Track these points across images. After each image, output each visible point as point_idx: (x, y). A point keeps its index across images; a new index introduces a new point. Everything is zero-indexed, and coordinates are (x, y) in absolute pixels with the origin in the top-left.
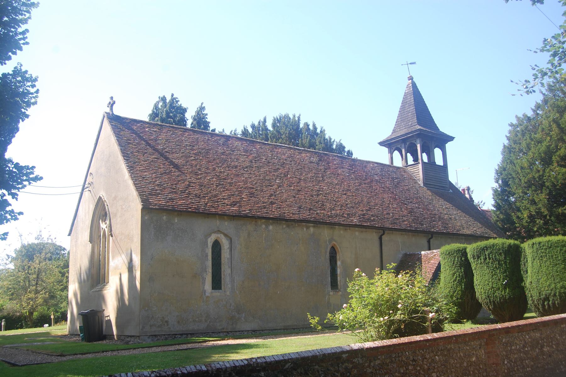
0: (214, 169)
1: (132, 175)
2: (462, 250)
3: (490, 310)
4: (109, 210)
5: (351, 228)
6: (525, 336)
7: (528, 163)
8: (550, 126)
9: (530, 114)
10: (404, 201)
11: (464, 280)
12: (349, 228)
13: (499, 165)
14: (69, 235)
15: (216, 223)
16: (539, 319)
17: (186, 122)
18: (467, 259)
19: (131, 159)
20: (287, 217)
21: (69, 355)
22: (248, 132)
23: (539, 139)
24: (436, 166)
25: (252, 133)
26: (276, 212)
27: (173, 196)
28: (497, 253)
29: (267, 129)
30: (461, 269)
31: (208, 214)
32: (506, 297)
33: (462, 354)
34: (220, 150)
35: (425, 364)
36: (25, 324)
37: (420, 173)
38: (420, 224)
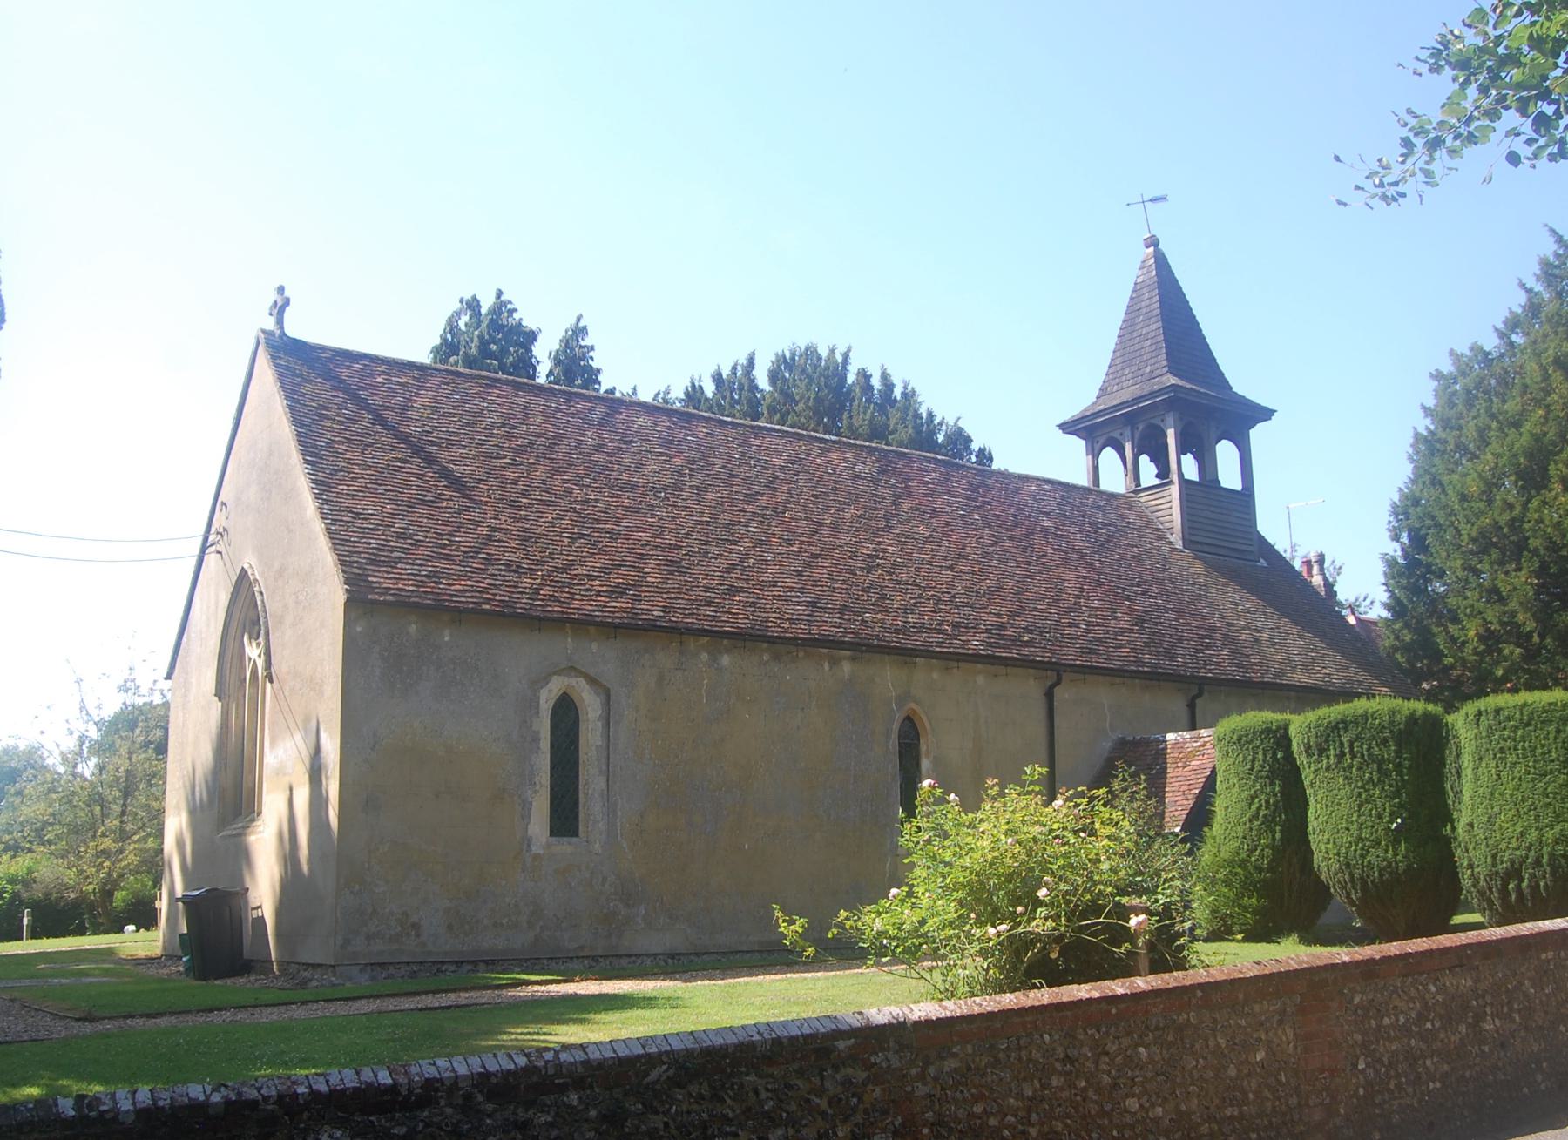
0: (569, 492)
1: (325, 507)
2: (1277, 731)
3: (1352, 903)
6: (1425, 986)
7: (1481, 484)
8: (1546, 377)
9: (1491, 343)
10: (1123, 590)
11: (1280, 816)
12: (956, 664)
13: (1401, 489)
15: (566, 645)
17: (535, 369)
18: (1290, 758)
19: (325, 462)
22: (703, 392)
23: (1513, 416)
24: (1223, 493)
26: (741, 616)
27: (440, 567)
29: (754, 388)
30: (1272, 784)
31: (540, 619)
32: (1397, 868)
35: (1104, 1072)
36: (91, 923)
37: (1173, 509)
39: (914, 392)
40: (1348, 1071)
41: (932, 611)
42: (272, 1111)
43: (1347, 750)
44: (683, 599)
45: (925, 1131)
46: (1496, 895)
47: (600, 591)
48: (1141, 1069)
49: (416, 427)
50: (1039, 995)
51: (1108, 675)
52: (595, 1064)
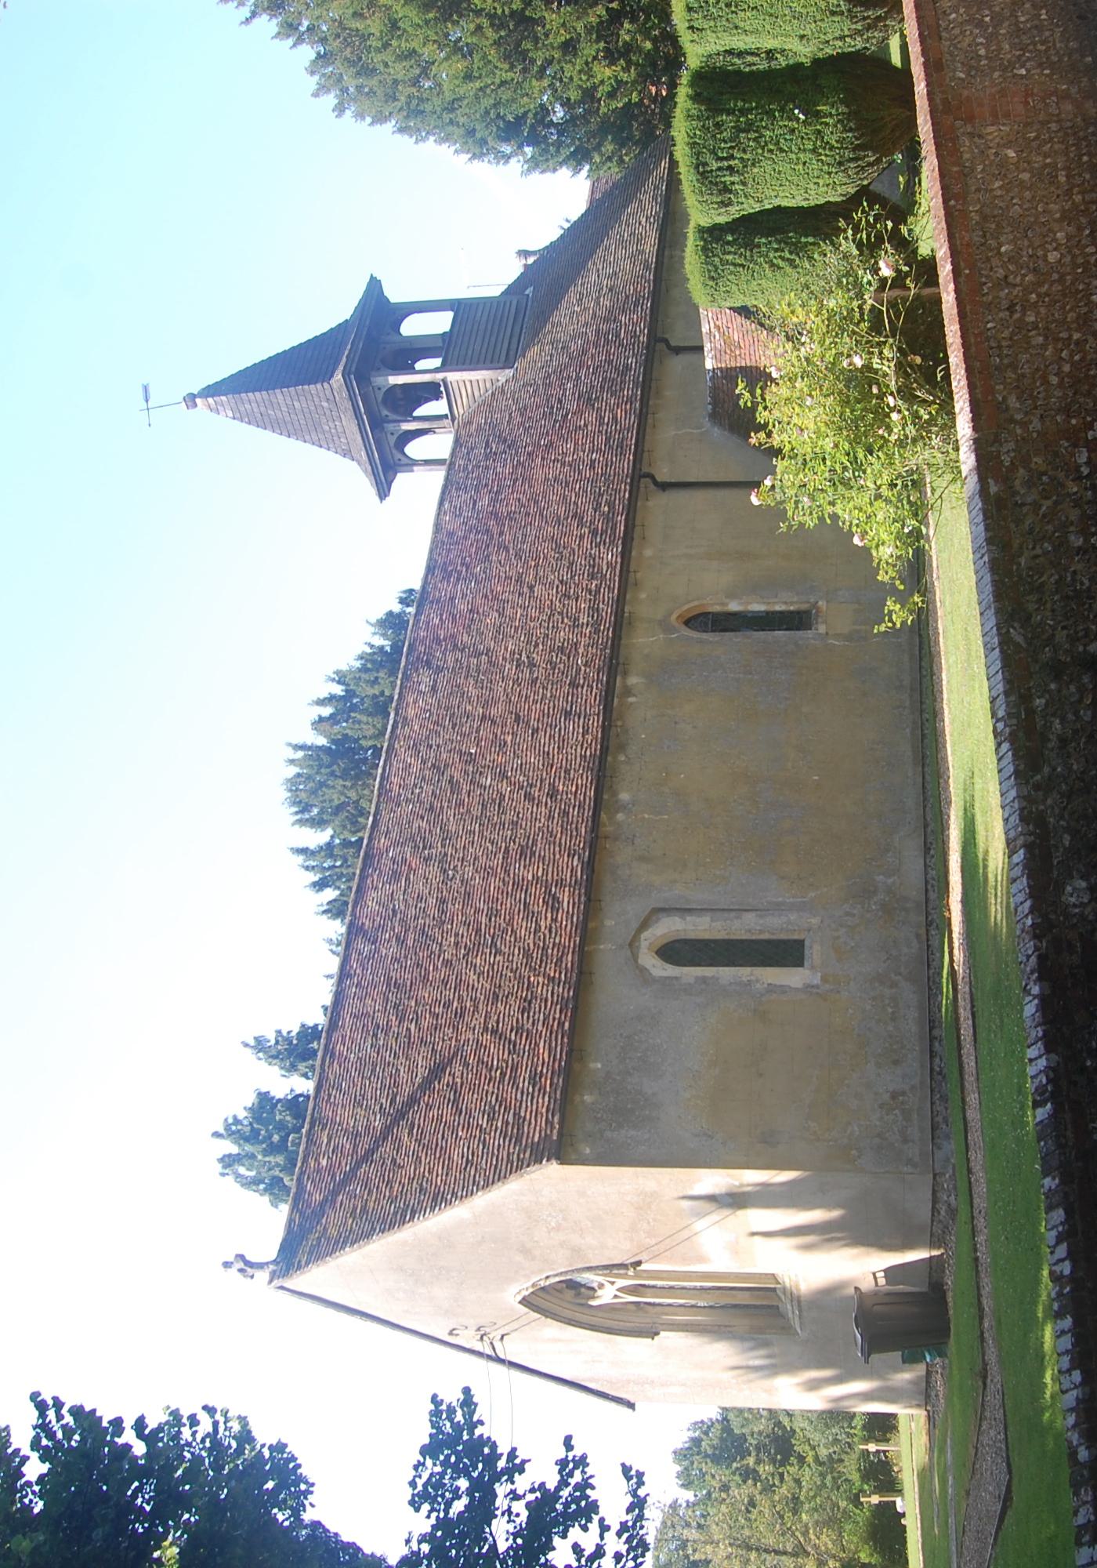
0: (447, 963)
1: (459, 1194)
2: (705, 240)
3: (878, 161)
4: (561, 1273)
5: (632, 570)
6: (950, 22)
7: (454, 58)
9: (307, 52)
10: (556, 421)
11: (791, 238)
12: (632, 575)
14: (631, 1406)
15: (607, 951)
16: (911, 28)
17: (300, 1095)
18: (734, 226)
20: (595, 750)
21: (983, 1355)
23: (385, 25)
25: (339, 888)
26: (580, 781)
27: (524, 1075)
28: (714, 136)
30: (759, 246)
31: (580, 973)
32: (844, 114)
33: (997, 184)
34: (390, 950)
35: (1023, 280)
37: (473, 378)
38: (624, 374)
39: (337, 672)
40: (1027, 82)
41: (577, 601)
42: (1048, 942)
43: (726, 164)
44: (560, 839)
45: (1074, 422)
46: (870, 13)
47: (552, 919)
48: (1021, 250)
49: (375, 1121)
50: (951, 334)
51: (645, 430)
52: (1008, 687)
